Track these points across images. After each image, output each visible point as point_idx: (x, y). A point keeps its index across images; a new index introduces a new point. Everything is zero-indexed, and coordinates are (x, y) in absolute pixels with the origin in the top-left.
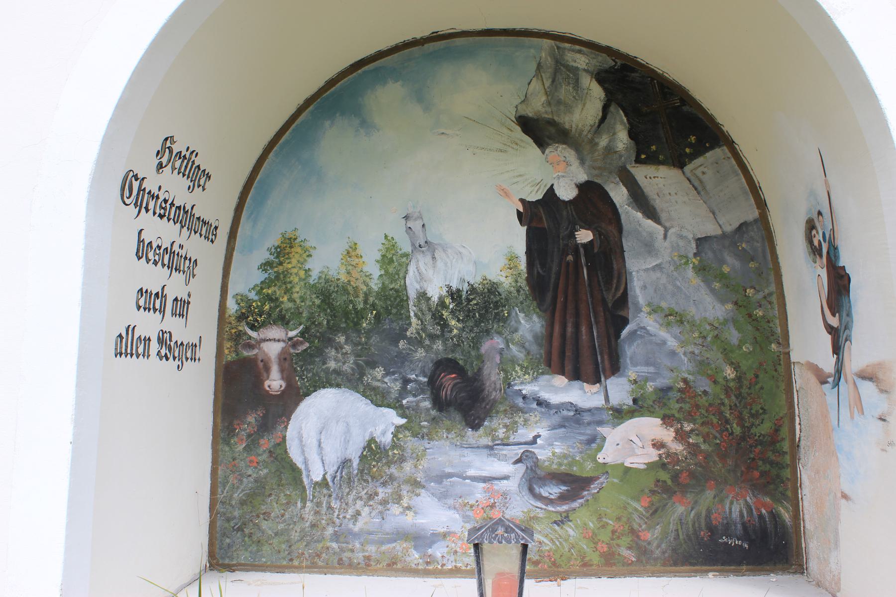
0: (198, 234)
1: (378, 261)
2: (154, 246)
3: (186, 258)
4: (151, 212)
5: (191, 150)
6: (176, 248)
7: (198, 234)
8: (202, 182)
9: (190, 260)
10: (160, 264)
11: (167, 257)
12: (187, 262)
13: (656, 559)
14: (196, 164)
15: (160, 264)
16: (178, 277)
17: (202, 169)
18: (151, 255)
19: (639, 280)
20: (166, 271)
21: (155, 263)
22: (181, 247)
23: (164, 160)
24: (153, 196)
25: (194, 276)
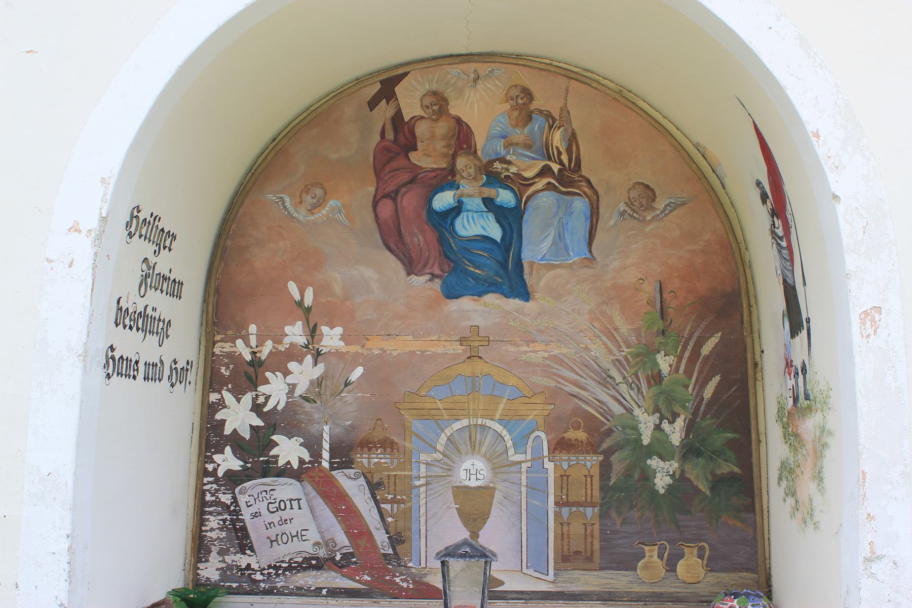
0: (159, 291)
1: (816, 525)
2: (130, 311)
3: (159, 320)
4: (165, 293)
5: (154, 215)
6: (149, 311)
7: (159, 291)
8: (168, 244)
9: (164, 321)
10: (135, 329)
11: (141, 321)
12: (161, 324)
13: (224, 561)
14: (160, 228)
15: (135, 329)
16: (153, 339)
17: (166, 231)
18: (127, 322)
19: (661, 343)
20: (141, 334)
21: (131, 328)
22: (154, 309)
23: (133, 230)
24: (165, 279)
25: (167, 337)
